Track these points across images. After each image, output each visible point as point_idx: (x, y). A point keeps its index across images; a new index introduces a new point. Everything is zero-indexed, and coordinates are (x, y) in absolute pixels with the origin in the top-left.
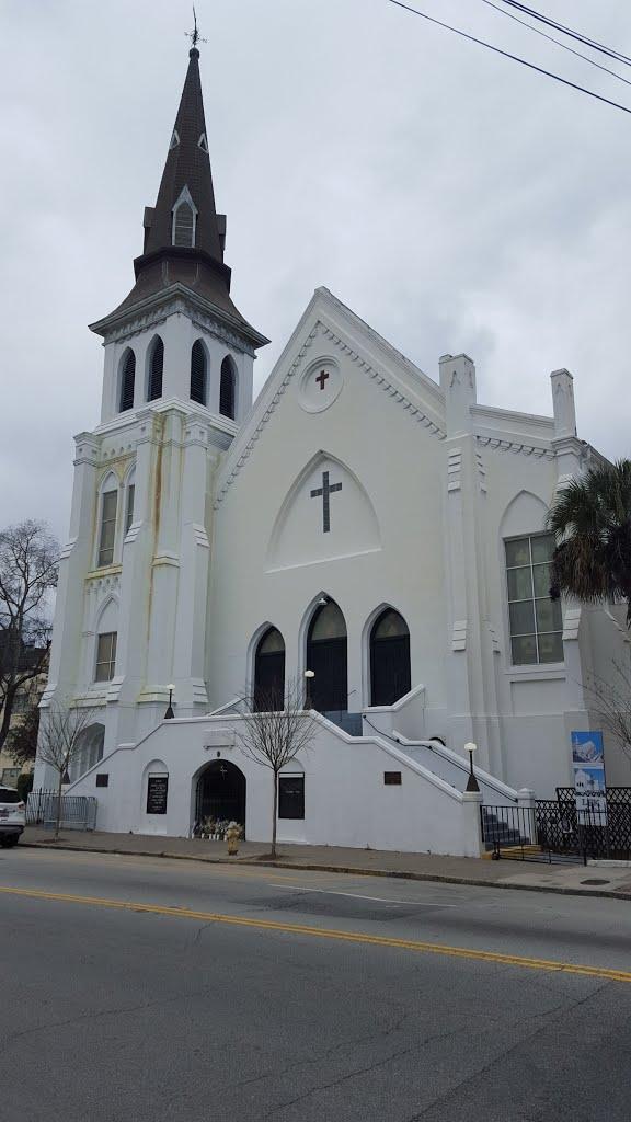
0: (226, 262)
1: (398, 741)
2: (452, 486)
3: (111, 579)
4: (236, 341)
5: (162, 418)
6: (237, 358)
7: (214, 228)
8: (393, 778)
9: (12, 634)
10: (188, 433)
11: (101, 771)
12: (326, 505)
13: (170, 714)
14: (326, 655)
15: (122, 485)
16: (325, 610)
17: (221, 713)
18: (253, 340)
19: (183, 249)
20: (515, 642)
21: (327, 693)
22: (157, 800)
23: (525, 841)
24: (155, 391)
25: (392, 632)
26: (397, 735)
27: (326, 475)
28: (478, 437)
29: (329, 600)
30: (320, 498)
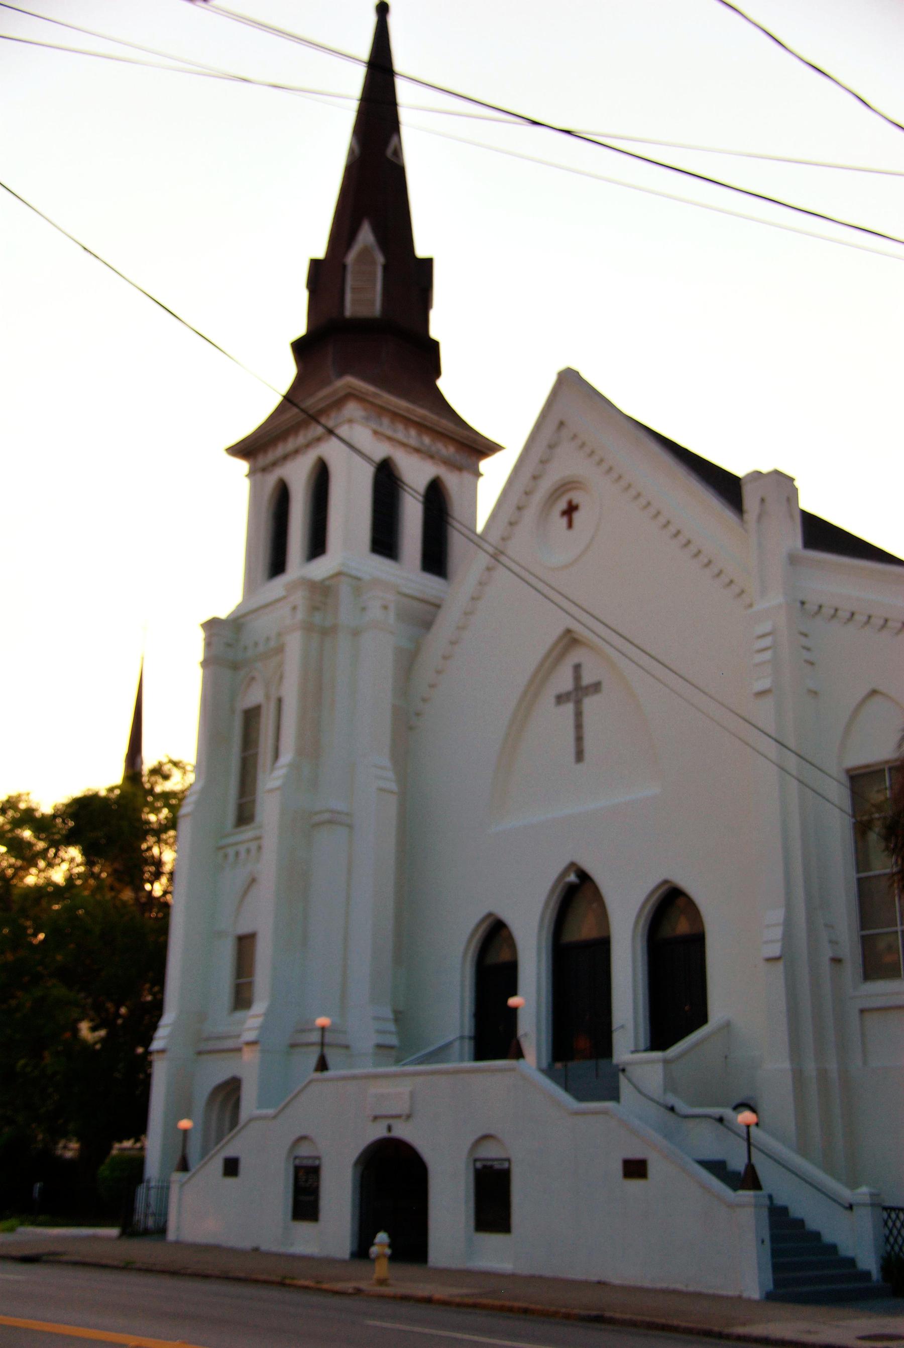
0: (435, 332)
1: (672, 1109)
2: (759, 686)
3: (253, 846)
4: (448, 451)
5: (322, 593)
6: (452, 481)
7: (412, 281)
8: (635, 1169)
9: (903, 880)
10: (364, 609)
11: (230, 1151)
12: (579, 715)
14: (579, 967)
15: (267, 697)
16: (577, 893)
18: (479, 448)
19: (370, 316)
20: (867, 944)
21: (580, 1035)
22: (305, 1202)
23: (867, 1275)
24: (317, 545)
25: (683, 927)
26: (672, 1100)
27: (577, 668)
28: (803, 603)
29: (584, 876)
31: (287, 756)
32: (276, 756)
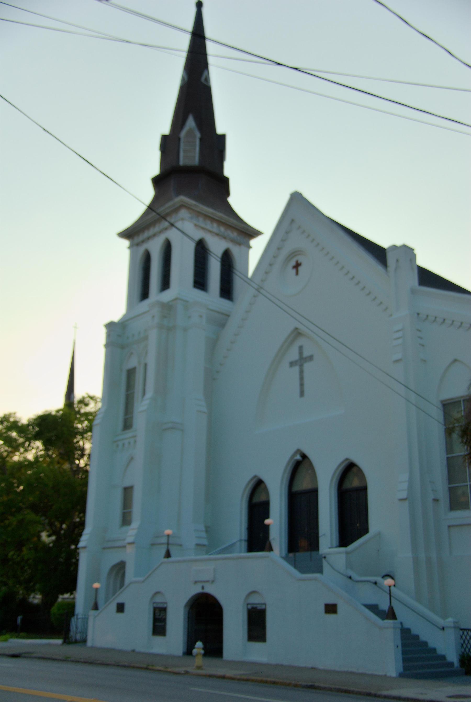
0: (227, 173)
1: (350, 578)
4: (234, 235)
5: (168, 309)
6: (235, 251)
7: (215, 146)
8: (331, 609)
10: (190, 317)
11: (120, 600)
12: (301, 372)
13: (168, 555)
14: (302, 504)
16: (300, 464)
17: (219, 553)
18: (250, 233)
19: (193, 166)
20: (452, 491)
21: (302, 537)
22: (159, 626)
23: (451, 664)
24: (165, 284)
26: (350, 573)
27: (301, 348)
28: (418, 314)
29: (304, 456)
30: (296, 369)
31: (149, 394)
32: (144, 393)
